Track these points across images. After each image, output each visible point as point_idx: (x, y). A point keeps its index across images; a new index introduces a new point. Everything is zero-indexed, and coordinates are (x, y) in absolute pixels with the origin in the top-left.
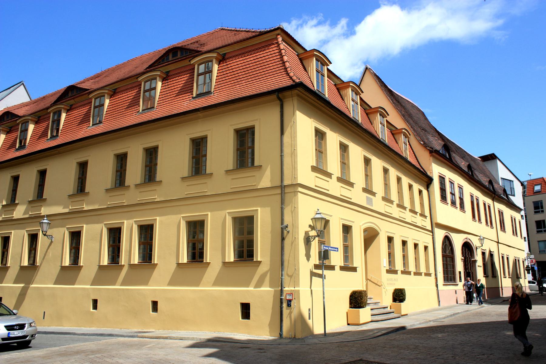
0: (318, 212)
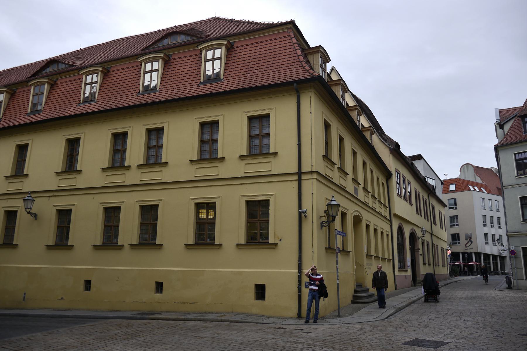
0: (333, 199)
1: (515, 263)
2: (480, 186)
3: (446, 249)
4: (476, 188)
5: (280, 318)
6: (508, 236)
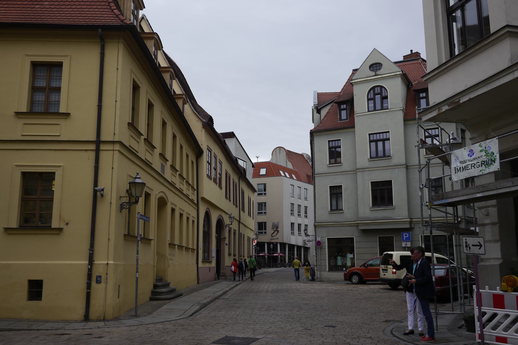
0: (138, 176)
1: (319, 255)
2: (290, 172)
3: (252, 239)
4: (287, 174)
5: (60, 322)
6: (315, 226)
